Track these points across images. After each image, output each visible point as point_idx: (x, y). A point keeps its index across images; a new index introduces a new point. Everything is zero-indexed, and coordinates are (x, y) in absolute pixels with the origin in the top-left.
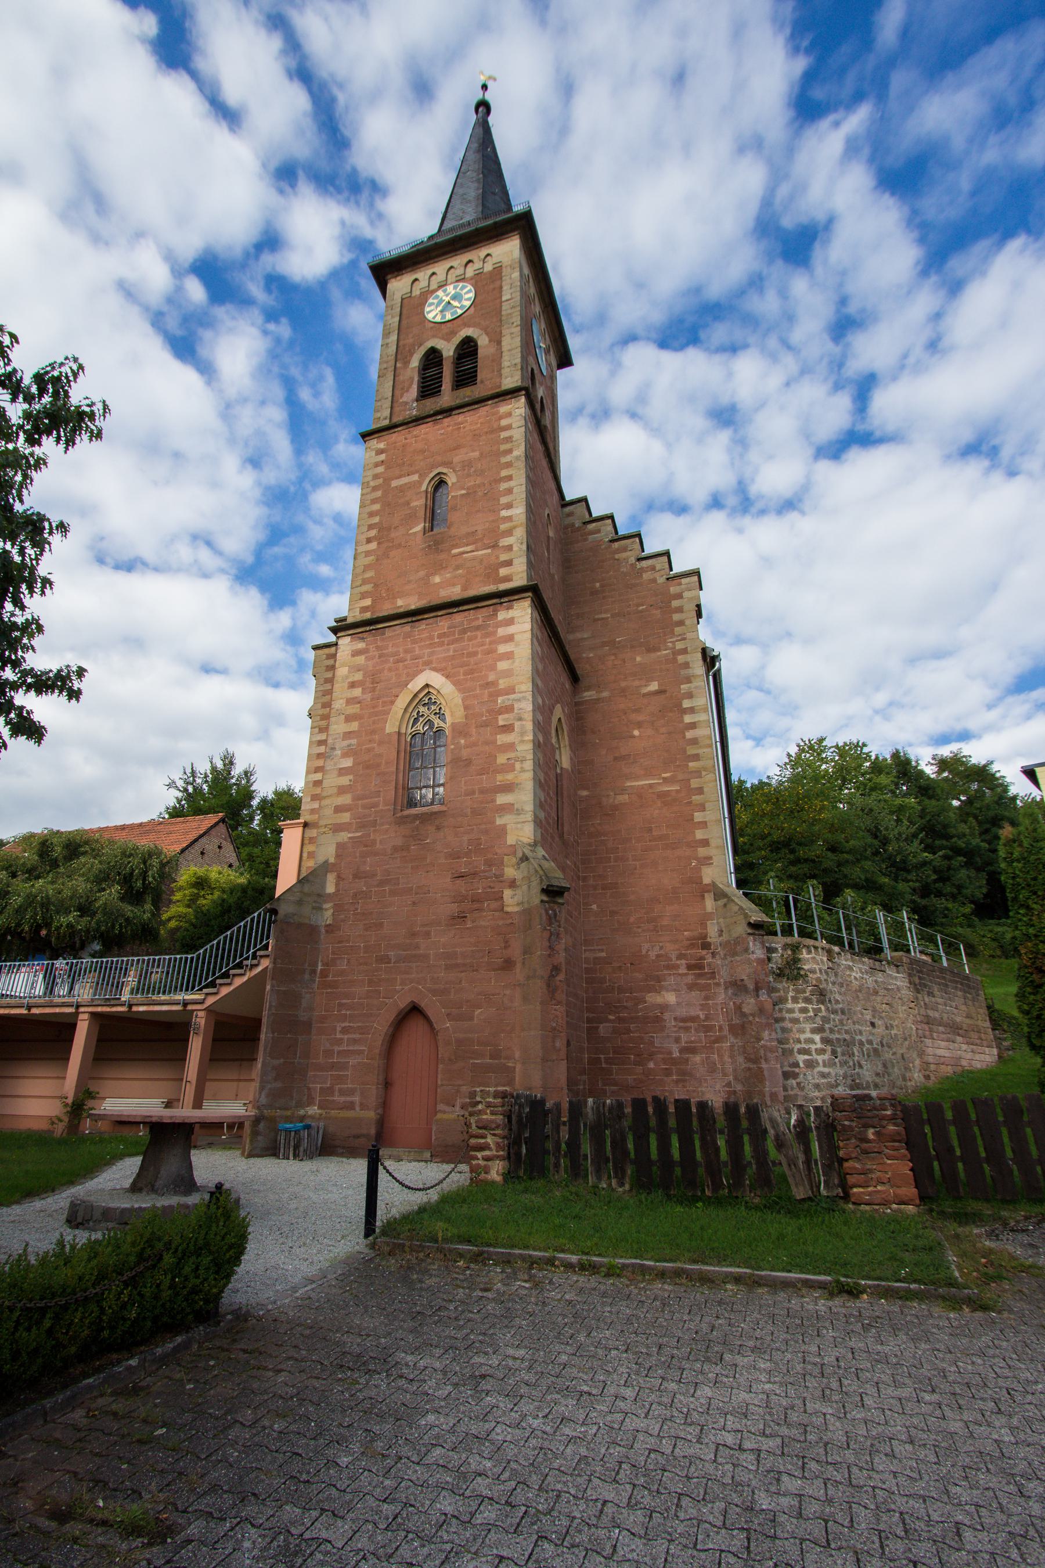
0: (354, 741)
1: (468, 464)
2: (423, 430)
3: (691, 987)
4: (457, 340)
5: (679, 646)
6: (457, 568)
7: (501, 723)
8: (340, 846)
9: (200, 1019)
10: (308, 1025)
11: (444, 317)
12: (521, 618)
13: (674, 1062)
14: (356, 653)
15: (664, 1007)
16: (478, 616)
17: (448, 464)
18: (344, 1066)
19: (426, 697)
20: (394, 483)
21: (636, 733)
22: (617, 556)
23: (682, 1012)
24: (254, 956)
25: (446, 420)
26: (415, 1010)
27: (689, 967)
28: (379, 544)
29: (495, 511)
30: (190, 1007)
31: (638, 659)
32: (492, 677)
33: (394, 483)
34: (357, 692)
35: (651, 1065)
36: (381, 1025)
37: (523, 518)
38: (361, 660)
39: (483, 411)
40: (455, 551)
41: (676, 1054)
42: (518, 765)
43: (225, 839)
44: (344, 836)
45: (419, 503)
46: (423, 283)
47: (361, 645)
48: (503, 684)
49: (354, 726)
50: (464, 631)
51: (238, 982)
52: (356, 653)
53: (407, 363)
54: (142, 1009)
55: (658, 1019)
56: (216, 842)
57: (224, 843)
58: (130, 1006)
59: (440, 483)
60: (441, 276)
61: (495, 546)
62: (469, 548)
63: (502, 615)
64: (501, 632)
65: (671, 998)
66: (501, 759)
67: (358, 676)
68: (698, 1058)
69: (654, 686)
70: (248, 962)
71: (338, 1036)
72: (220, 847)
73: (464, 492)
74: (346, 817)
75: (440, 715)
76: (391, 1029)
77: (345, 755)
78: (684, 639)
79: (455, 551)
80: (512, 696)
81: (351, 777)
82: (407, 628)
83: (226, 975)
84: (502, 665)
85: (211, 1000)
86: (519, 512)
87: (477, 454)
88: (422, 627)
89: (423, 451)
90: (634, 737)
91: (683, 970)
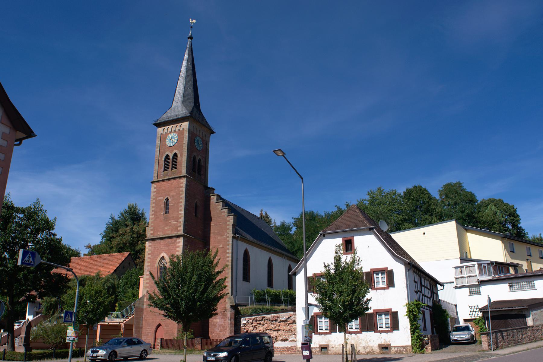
1: (173, 196)
2: (164, 183)
3: (222, 318)
4: (173, 153)
9: (123, 326)
10: (142, 328)
12: (181, 240)
13: (217, 334)
14: (150, 246)
15: (217, 322)
16: (174, 239)
17: (169, 195)
18: (148, 335)
19: (163, 258)
20: (158, 199)
23: (220, 323)
29: (178, 212)
33: (158, 199)
34: (150, 256)
36: (154, 328)
37: (183, 215)
38: (150, 248)
39: (177, 180)
45: (163, 206)
46: (165, 131)
51: (130, 318)
53: (162, 158)
55: (215, 325)
59: (167, 200)
60: (170, 130)
65: (218, 320)
67: (150, 252)
68: (222, 333)
69: (221, 246)
72: (129, 264)
76: (233, 321)
86: (182, 212)
87: (175, 194)
88: (163, 241)
89: (164, 190)
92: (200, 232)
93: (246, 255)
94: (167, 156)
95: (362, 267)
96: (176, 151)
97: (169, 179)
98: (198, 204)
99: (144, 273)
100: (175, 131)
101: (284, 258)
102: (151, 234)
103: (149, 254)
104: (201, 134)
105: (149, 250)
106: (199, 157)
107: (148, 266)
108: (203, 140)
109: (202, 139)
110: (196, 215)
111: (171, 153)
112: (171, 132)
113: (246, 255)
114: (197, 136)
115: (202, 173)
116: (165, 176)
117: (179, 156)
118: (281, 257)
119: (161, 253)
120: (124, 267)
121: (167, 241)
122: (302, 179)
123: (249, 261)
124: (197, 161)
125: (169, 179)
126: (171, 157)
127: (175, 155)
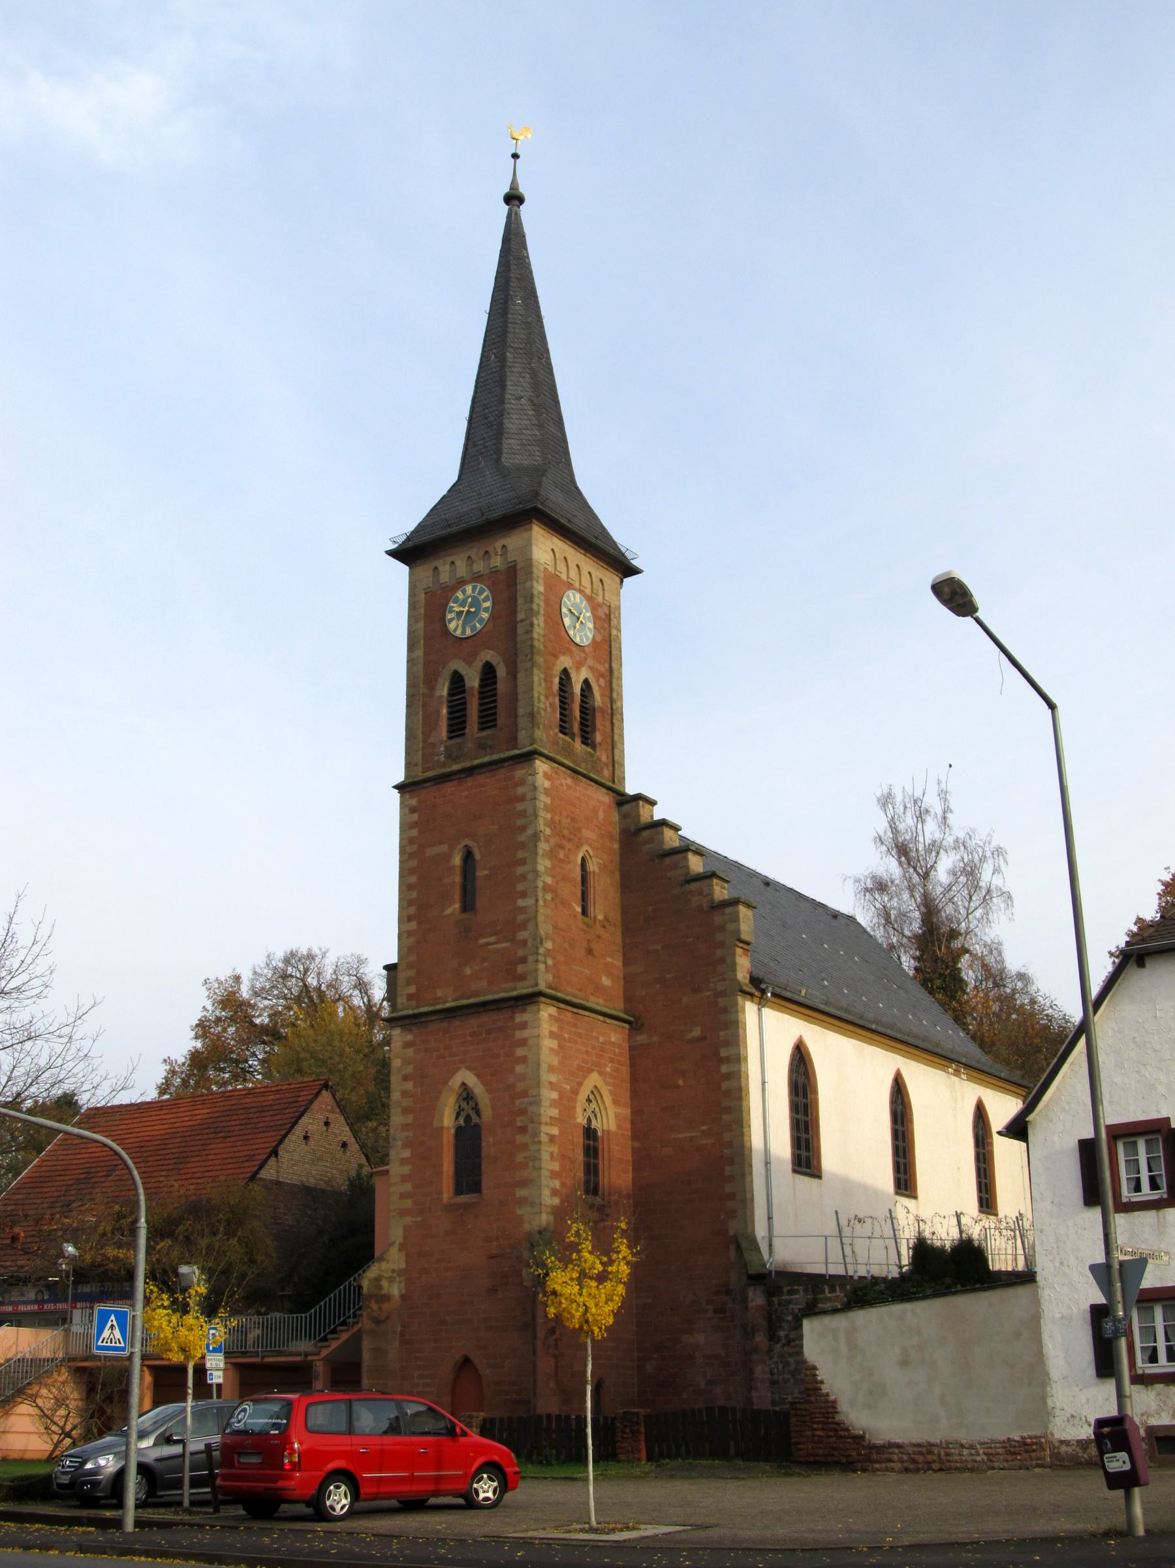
0: (410, 1134)
4: (478, 665)
5: (720, 987)
6: (484, 960)
7: (519, 1124)
8: (406, 1229)
11: (464, 632)
14: (407, 1045)
19: (467, 1095)
20: (430, 852)
21: (681, 1082)
22: (668, 874)
24: (355, 1316)
25: (469, 779)
26: (467, 1361)
27: (716, 1311)
28: (419, 924)
30: (310, 1358)
31: (685, 1000)
32: (511, 1080)
33: (430, 852)
34: (409, 1085)
35: (684, 1396)
38: (410, 1052)
39: (502, 774)
40: (482, 941)
41: (703, 1385)
42: (531, 1164)
43: (332, 1111)
44: (409, 1220)
47: (409, 1037)
48: (520, 1087)
49: (410, 1119)
50: (489, 1032)
52: (407, 1045)
54: (271, 1359)
56: (321, 1117)
57: (332, 1116)
58: (263, 1357)
61: (513, 940)
62: (492, 939)
63: (519, 1018)
64: (519, 1035)
65: (700, 1339)
66: (519, 1157)
67: (409, 1069)
69: (697, 1032)
70: (351, 1320)
71: (416, 1381)
72: (327, 1124)
73: (486, 872)
74: (408, 1203)
75: (478, 1112)
77: (405, 1146)
78: (724, 980)
79: (482, 941)
80: (526, 1100)
81: (410, 1167)
82: (445, 1024)
83: (334, 1331)
84: (519, 1069)
85: (325, 1352)
90: (678, 1087)
91: (710, 1314)
92: (606, 981)
93: (899, 1092)
94: (457, 681)
95: (217, 979)
96: (489, 655)
97: (470, 771)
98: (592, 867)
99: (392, 1153)
100: (476, 578)
101: (957, 1073)
102: (410, 997)
103: (406, 1078)
104: (586, 580)
105: (406, 1061)
106: (584, 673)
107: (405, 1127)
108: (594, 606)
109: (590, 599)
110: (584, 912)
111: (469, 663)
112: (461, 583)
113: (899, 1092)
114: (570, 586)
115: (598, 737)
116: (451, 756)
117: (501, 672)
118: (943, 1068)
119: (453, 1072)
120: (306, 1138)
121: (474, 1023)
122: (1052, 706)
123: (815, 1091)
124: (577, 689)
125: (470, 771)
126: (473, 681)
127: (488, 672)
